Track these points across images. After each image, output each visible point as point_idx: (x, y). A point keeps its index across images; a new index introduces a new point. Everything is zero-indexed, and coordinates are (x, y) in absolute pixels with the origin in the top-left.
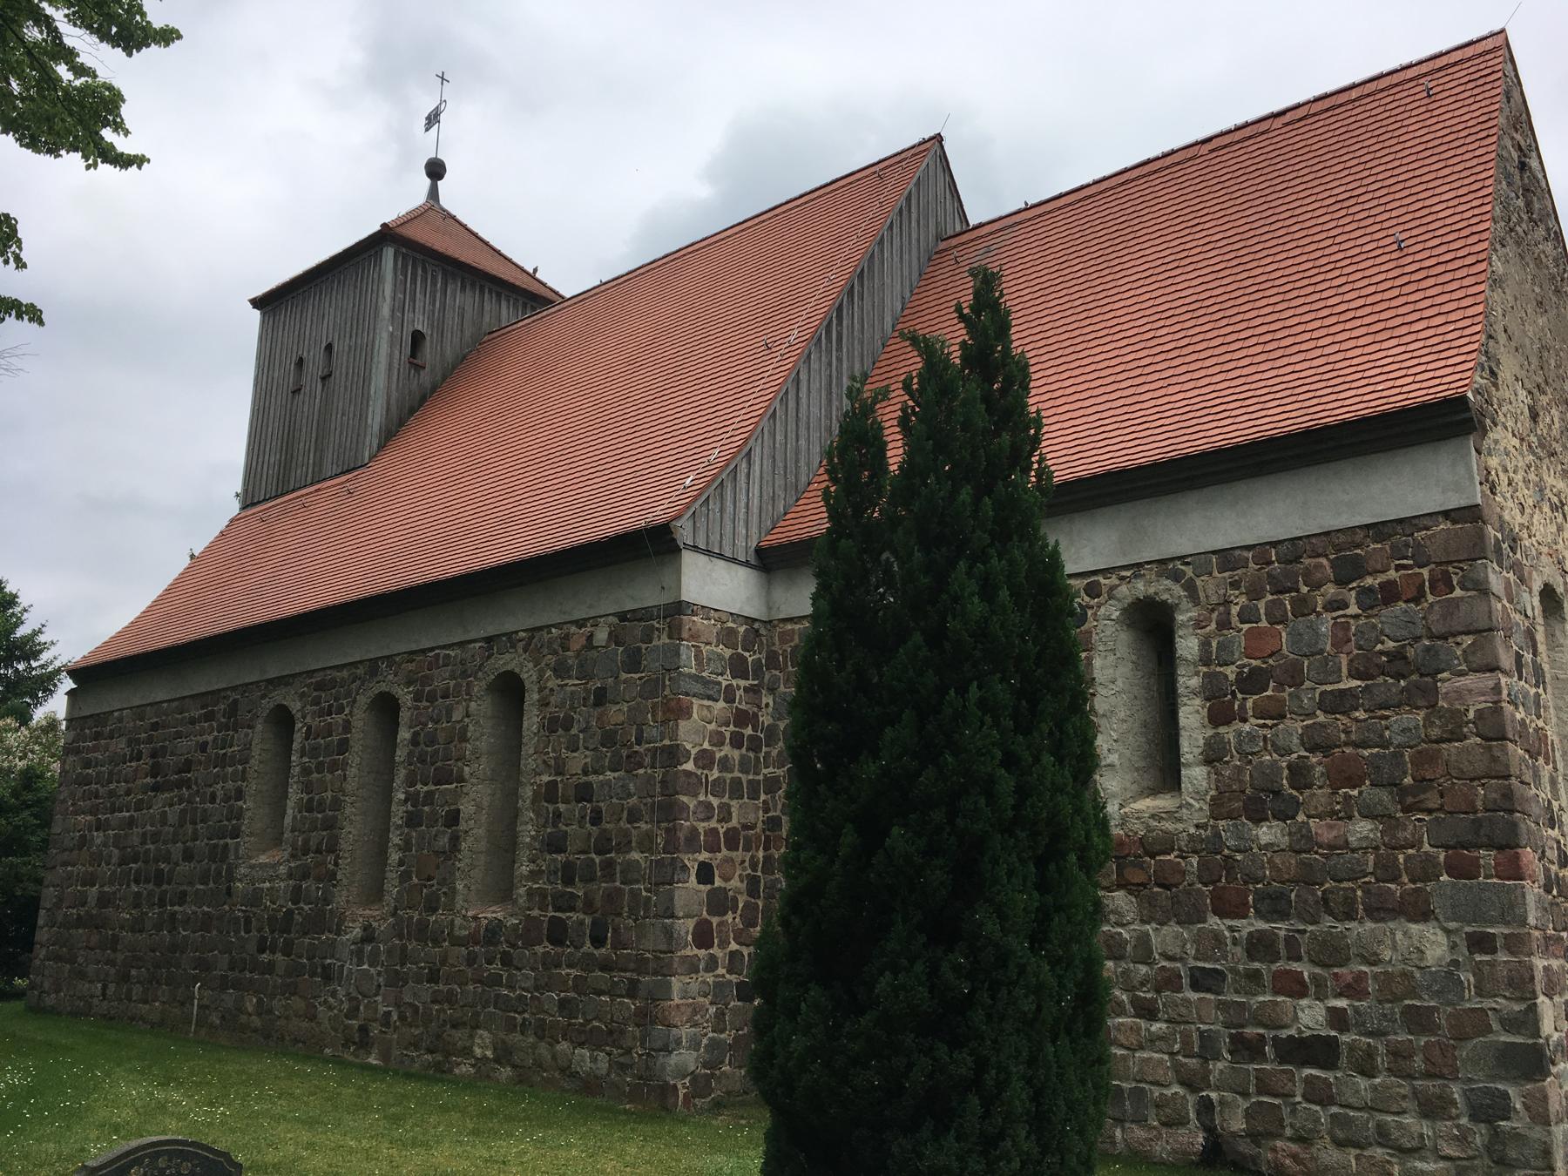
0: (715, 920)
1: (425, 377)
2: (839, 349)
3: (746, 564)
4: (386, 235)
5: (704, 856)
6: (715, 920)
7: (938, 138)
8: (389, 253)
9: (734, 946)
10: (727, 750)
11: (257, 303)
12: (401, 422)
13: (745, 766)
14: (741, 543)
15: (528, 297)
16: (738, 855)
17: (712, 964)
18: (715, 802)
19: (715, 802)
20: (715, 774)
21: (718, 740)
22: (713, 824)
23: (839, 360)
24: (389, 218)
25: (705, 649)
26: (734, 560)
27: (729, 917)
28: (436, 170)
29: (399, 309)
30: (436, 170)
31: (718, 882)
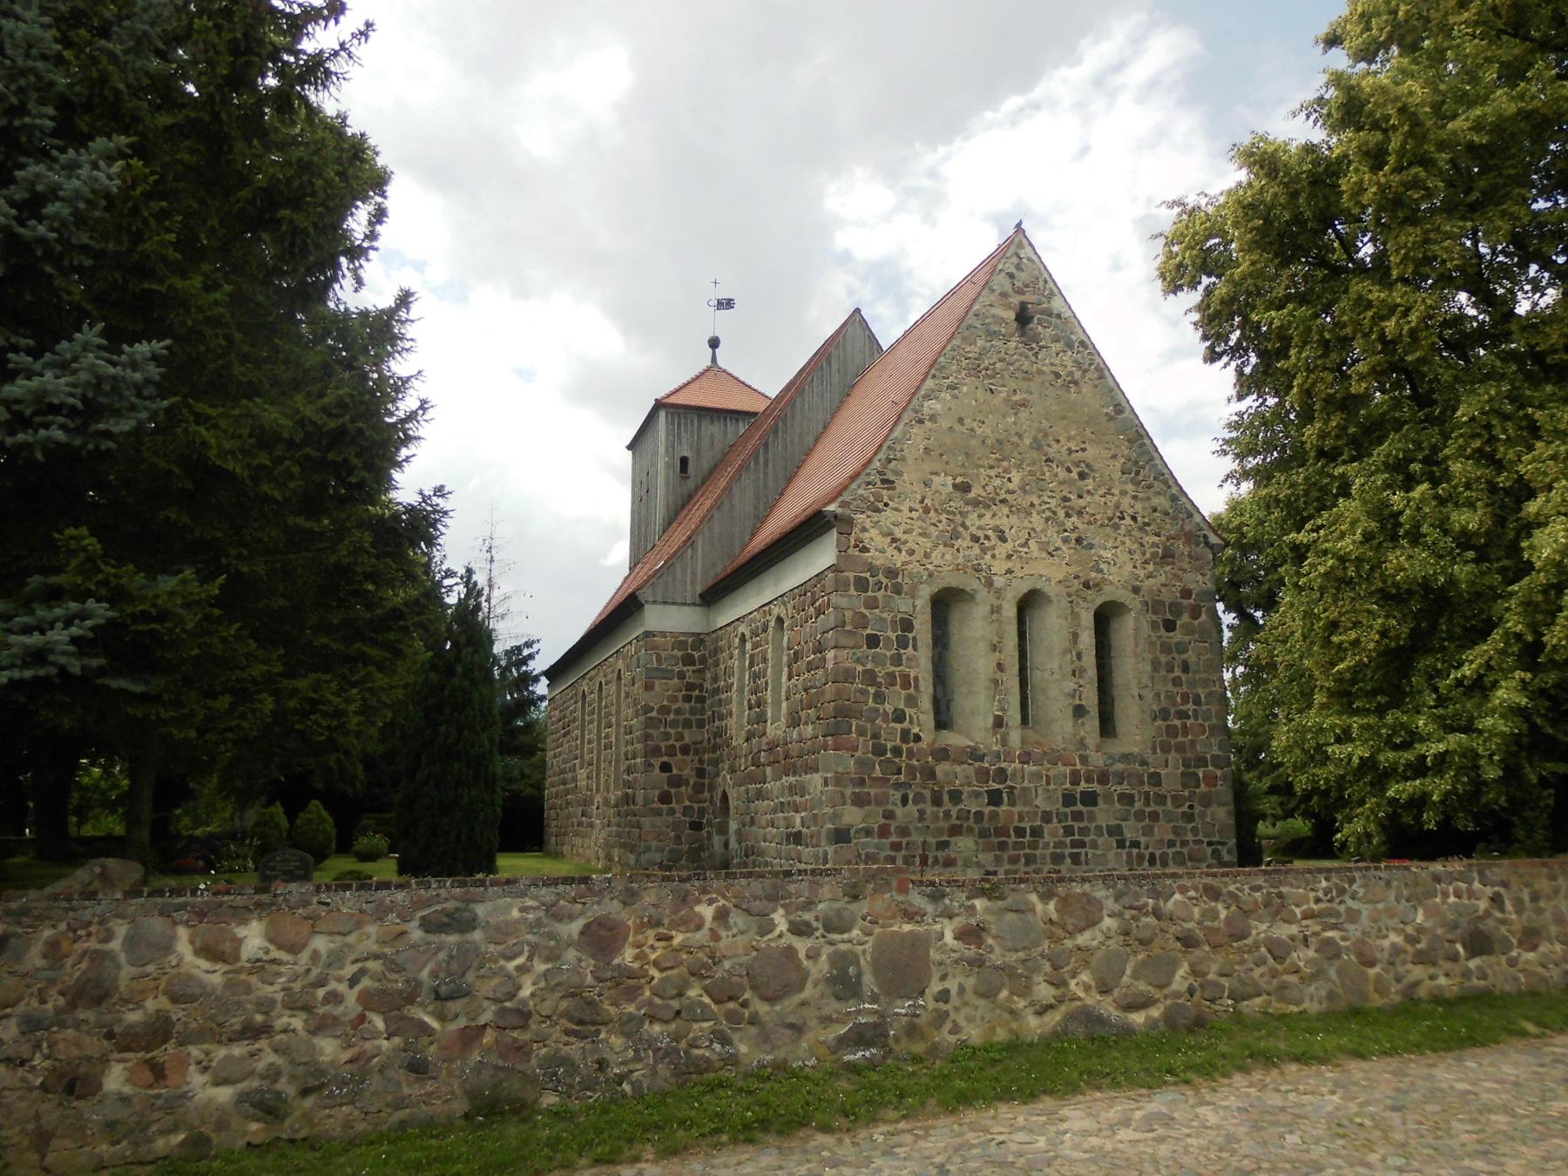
0: (673, 791)
1: (691, 484)
2: (766, 465)
3: (694, 604)
4: (659, 405)
5: (665, 759)
6: (673, 791)
7: (857, 311)
8: (662, 414)
9: (687, 803)
10: (680, 704)
11: (629, 447)
12: (677, 514)
13: (692, 712)
14: (689, 594)
15: (755, 414)
16: (689, 758)
17: (672, 812)
18: (672, 731)
19: (672, 731)
20: (672, 716)
21: (674, 699)
22: (671, 742)
23: (766, 474)
24: (660, 394)
25: (663, 654)
26: (684, 604)
27: (683, 789)
28: (714, 343)
29: (670, 448)
30: (714, 343)
31: (675, 771)
